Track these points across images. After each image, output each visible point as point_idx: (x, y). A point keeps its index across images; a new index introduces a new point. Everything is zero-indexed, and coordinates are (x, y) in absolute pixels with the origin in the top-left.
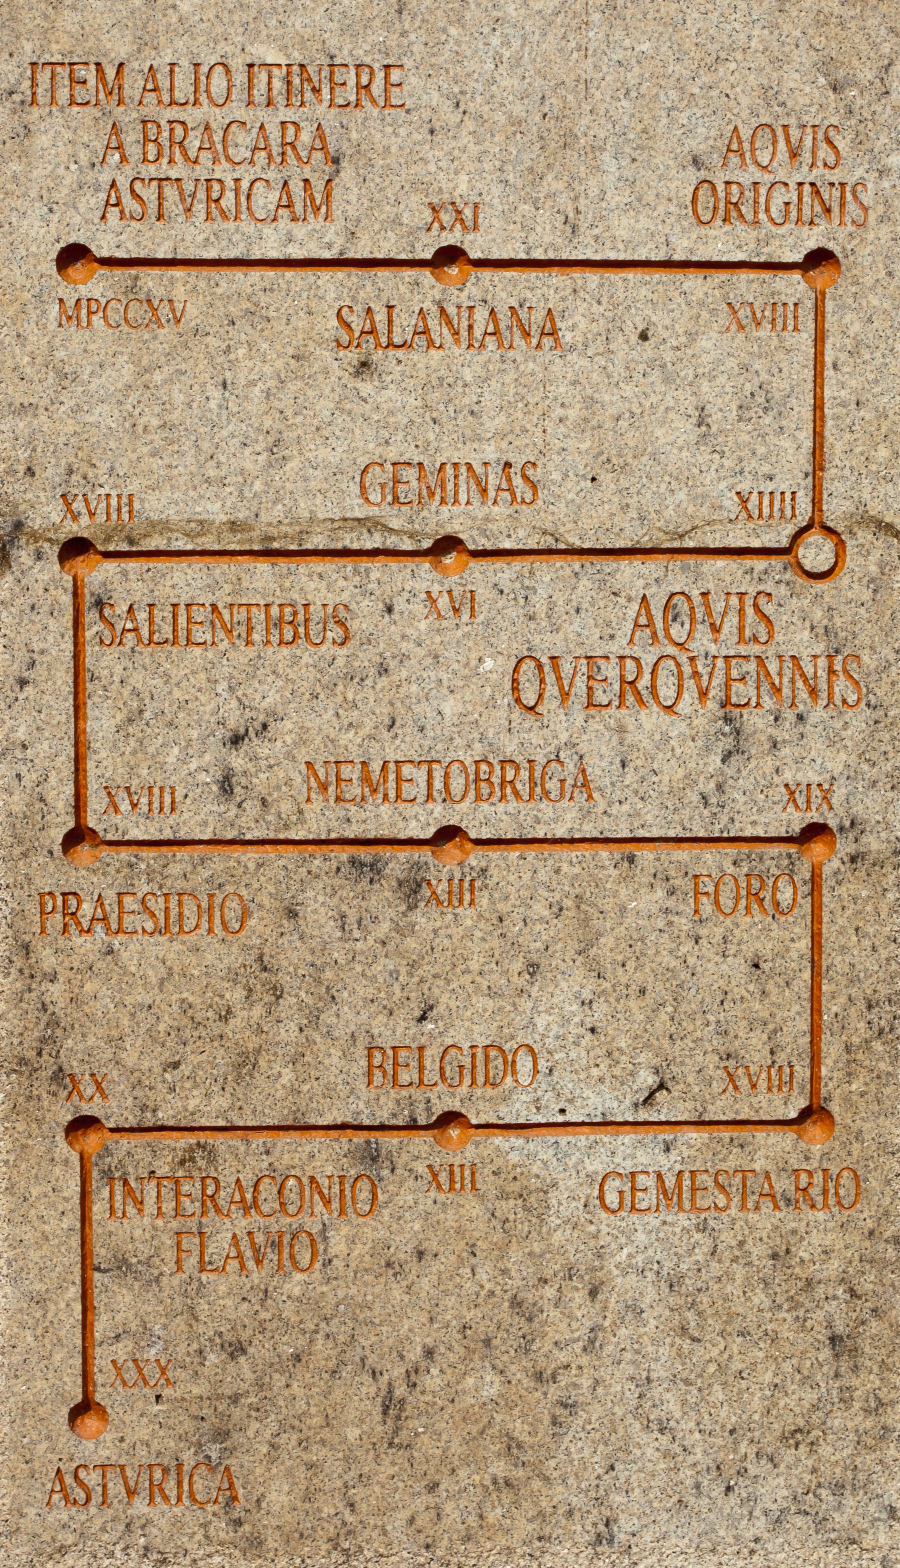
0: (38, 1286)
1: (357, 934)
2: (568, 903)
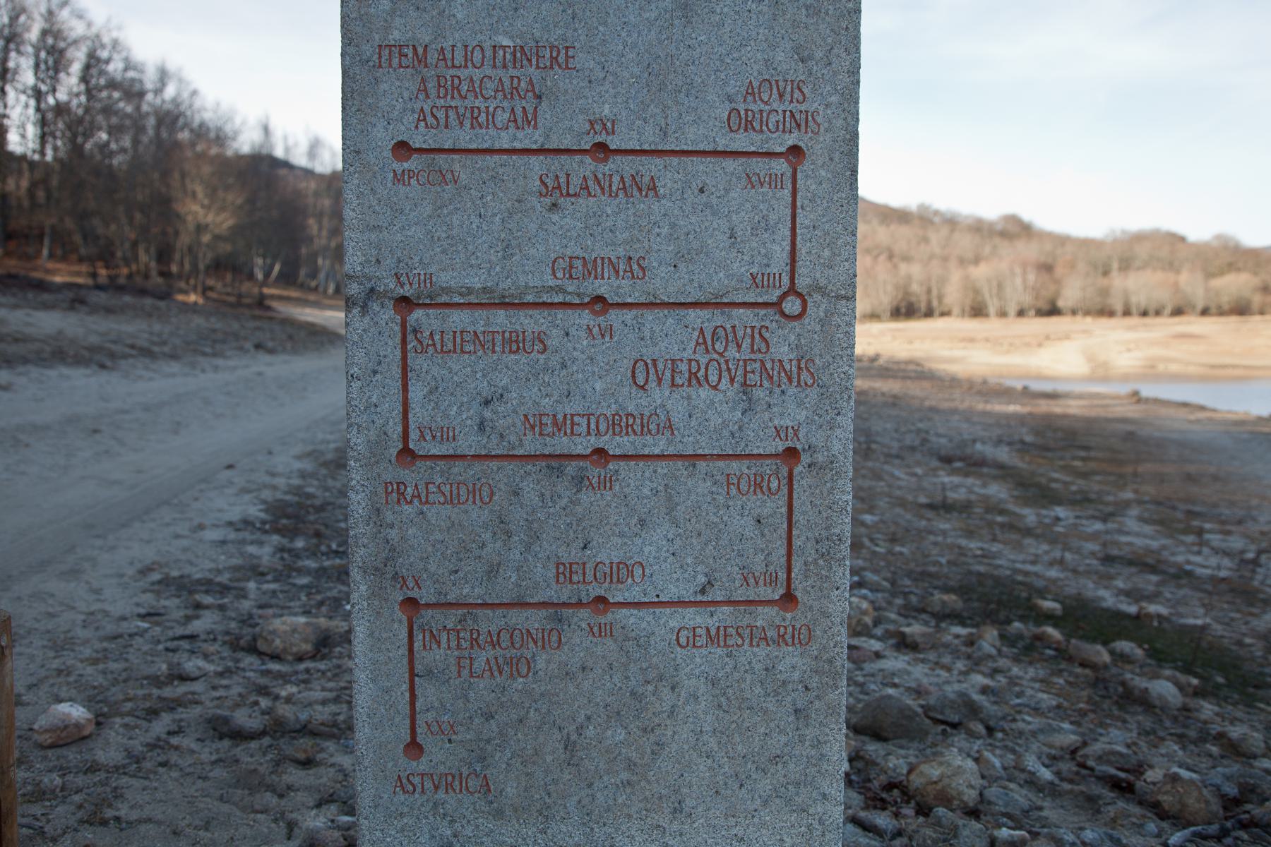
0: (387, 684)
1: (550, 504)
2: (660, 488)
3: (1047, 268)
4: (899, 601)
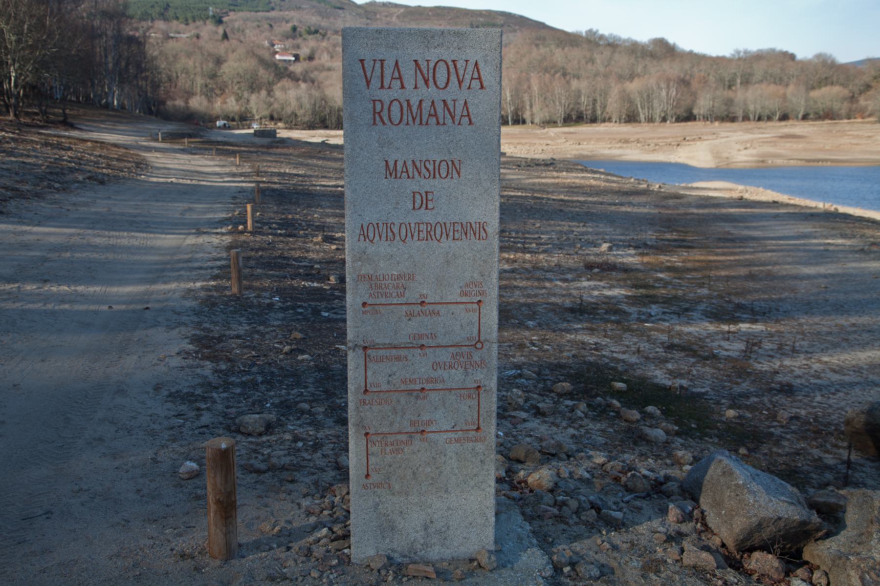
3: (684, 82)
4: (541, 385)
